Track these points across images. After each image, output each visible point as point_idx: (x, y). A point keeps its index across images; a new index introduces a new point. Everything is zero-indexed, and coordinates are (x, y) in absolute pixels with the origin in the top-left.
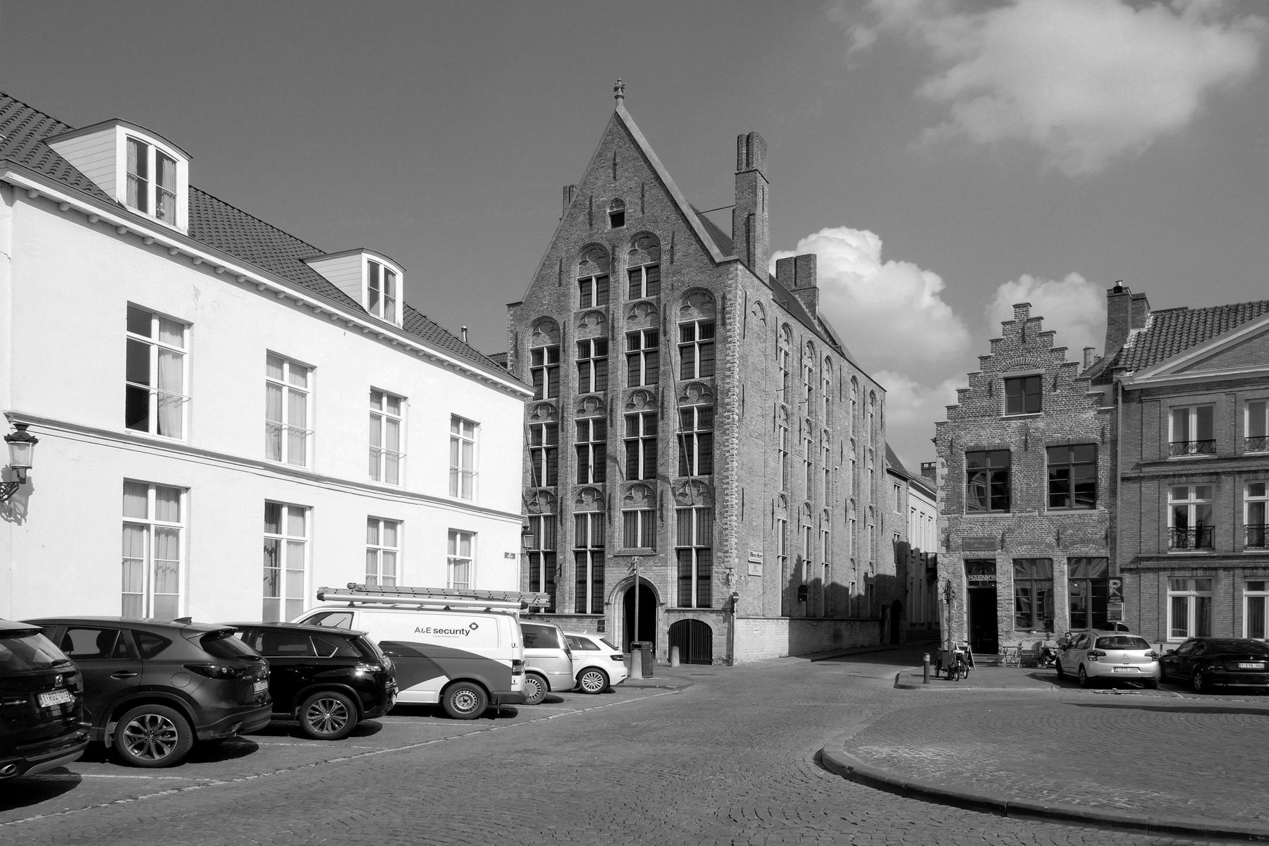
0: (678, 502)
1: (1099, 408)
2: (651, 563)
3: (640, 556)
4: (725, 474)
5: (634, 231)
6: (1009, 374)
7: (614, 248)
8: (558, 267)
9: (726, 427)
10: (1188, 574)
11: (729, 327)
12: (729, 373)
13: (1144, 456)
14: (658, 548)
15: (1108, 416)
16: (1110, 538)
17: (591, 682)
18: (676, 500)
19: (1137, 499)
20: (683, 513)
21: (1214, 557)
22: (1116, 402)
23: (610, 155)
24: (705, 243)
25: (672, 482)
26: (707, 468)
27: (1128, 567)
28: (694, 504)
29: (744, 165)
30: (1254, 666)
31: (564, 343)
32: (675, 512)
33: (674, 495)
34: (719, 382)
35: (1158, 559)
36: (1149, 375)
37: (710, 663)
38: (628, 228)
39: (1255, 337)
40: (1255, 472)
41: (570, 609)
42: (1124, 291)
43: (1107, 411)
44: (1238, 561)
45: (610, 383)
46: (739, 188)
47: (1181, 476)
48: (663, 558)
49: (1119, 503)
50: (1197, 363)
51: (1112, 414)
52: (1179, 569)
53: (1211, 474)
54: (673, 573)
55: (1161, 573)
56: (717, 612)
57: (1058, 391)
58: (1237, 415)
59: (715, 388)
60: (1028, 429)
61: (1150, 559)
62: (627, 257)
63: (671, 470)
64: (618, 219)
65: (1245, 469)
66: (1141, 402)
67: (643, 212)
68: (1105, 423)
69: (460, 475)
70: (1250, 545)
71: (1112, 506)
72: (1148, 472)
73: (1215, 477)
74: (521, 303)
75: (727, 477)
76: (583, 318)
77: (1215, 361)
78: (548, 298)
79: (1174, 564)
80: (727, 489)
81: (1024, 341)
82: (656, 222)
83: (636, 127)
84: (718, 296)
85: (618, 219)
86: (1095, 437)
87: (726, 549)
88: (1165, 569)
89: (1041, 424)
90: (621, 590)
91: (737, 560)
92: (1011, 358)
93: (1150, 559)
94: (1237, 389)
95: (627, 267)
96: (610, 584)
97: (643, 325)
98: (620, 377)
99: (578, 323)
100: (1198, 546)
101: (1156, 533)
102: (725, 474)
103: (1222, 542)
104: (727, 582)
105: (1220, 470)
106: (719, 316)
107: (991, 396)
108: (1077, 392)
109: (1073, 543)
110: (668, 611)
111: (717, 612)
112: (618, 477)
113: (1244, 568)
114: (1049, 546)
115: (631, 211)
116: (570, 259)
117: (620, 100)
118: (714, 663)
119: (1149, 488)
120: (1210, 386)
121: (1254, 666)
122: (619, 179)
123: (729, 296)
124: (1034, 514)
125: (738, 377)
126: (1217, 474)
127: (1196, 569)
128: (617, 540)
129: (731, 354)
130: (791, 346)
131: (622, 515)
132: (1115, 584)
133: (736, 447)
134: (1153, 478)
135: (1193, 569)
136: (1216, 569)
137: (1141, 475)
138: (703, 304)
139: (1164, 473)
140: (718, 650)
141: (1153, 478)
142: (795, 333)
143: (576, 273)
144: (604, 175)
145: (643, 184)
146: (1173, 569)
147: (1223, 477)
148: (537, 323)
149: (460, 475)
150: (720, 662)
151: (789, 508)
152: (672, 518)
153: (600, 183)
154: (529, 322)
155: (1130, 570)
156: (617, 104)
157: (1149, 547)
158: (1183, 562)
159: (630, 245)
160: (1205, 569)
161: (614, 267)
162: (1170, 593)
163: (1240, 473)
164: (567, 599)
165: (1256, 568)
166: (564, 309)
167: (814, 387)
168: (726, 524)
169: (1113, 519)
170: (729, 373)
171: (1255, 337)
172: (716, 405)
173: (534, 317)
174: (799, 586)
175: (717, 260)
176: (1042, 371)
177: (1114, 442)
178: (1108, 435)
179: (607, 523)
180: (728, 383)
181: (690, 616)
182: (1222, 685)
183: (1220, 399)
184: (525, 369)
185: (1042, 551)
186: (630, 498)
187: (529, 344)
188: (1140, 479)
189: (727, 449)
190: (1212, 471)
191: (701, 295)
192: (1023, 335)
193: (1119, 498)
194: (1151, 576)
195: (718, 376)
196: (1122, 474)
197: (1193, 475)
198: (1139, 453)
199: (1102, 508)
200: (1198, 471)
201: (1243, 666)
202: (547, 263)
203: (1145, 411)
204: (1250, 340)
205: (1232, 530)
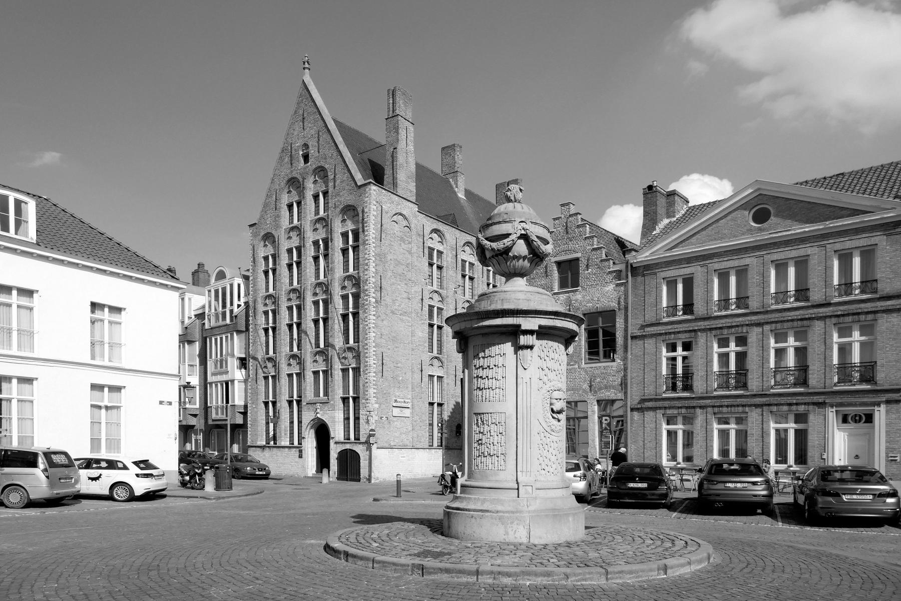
0: (342, 364)
1: (617, 282)
3: (321, 403)
4: (366, 342)
5: (314, 167)
6: (559, 259)
7: (304, 179)
8: (274, 197)
9: (366, 307)
10: (675, 412)
11: (366, 233)
12: (366, 267)
13: (646, 318)
14: (330, 397)
15: (622, 288)
16: (624, 385)
18: (341, 362)
19: (642, 353)
20: (345, 371)
21: (693, 398)
22: (627, 277)
23: (301, 112)
24: (353, 172)
25: (337, 349)
26: (357, 340)
27: (636, 407)
28: (350, 365)
29: (391, 112)
30: (640, 485)
31: (278, 251)
32: (340, 371)
33: (339, 358)
34: (361, 274)
35: (656, 400)
36: (647, 254)
37: (359, 480)
38: (312, 164)
39: (721, 219)
40: (721, 328)
42: (654, 189)
43: (622, 284)
44: (710, 401)
45: (303, 279)
46: (388, 131)
47: (670, 333)
48: (333, 404)
49: (630, 357)
50: (681, 242)
51: (625, 286)
52: (670, 408)
53: (690, 331)
54: (340, 415)
55: (658, 411)
56: (363, 443)
57: (590, 270)
58: (708, 283)
59: (359, 277)
60: (571, 301)
61: (650, 400)
63: (337, 340)
64: (306, 158)
65: (714, 326)
66: (644, 275)
67: (319, 152)
68: (621, 293)
69: (106, 346)
70: (720, 387)
71: (625, 359)
72: (648, 332)
73: (693, 334)
74: (255, 224)
75: (367, 344)
76: (289, 233)
77: (693, 240)
78: (269, 219)
79: (666, 404)
80: (367, 353)
81: (567, 233)
82: (325, 159)
83: (316, 90)
84: (360, 210)
85: (306, 158)
86: (614, 305)
87: (367, 397)
88: (660, 408)
89: (579, 296)
90: (311, 428)
91: (377, 406)
92: (559, 246)
93: (650, 400)
94: (708, 262)
95: (312, 193)
96: (305, 424)
97: (321, 235)
98: (308, 274)
99: (287, 237)
100: (736, 388)
101: (654, 380)
102: (366, 342)
103: (699, 386)
104: (368, 422)
105: (696, 328)
106: (361, 225)
107: (547, 276)
108: (602, 270)
109: (600, 389)
110: (336, 443)
111: (363, 443)
112: (308, 346)
113: (713, 407)
114: (584, 391)
115: (312, 152)
116: (282, 189)
117: (307, 70)
118: (362, 481)
119: (650, 344)
120: (689, 260)
121: (640, 485)
122: (306, 129)
123: (366, 210)
124: (575, 366)
125: (374, 270)
126: (695, 331)
127: (681, 408)
129: (368, 253)
130: (445, 246)
131: (312, 375)
132: (606, 420)
133: (373, 321)
134: (652, 336)
135: (679, 408)
136: (694, 407)
137: (644, 334)
138: (353, 217)
139: (659, 332)
140: (364, 472)
141: (652, 336)
142: (447, 236)
143: (285, 199)
144: (298, 126)
145: (319, 132)
146: (665, 408)
147: (699, 333)
148: (265, 238)
149: (106, 346)
150: (365, 480)
151: (445, 366)
152: (338, 375)
153: (296, 133)
154: (260, 237)
155: (637, 409)
156: (304, 74)
157: (650, 391)
158: (672, 403)
159: (313, 176)
160: (687, 408)
162: (773, 425)
163: (711, 329)
164: (283, 434)
165: (722, 406)
166: (278, 226)
168: (367, 379)
169: (625, 369)
170: (366, 267)
171: (721, 219)
173: (262, 234)
174: (456, 425)
175: (359, 184)
176: (579, 255)
177: (626, 308)
178: (623, 303)
179: (303, 380)
180: (366, 275)
181: (348, 446)
182: (616, 500)
183: (696, 270)
184: (259, 271)
185: (580, 395)
186: (315, 361)
187: (262, 253)
188: (642, 337)
189: (366, 323)
190: (691, 329)
191: (352, 211)
192: (566, 228)
193: (629, 353)
194: (651, 413)
195: (361, 270)
196: (632, 333)
197: (679, 332)
198: (643, 317)
199: (619, 361)
200: (681, 330)
201: (631, 485)
202: (269, 194)
203: (647, 283)
204: (717, 221)
205: (705, 376)
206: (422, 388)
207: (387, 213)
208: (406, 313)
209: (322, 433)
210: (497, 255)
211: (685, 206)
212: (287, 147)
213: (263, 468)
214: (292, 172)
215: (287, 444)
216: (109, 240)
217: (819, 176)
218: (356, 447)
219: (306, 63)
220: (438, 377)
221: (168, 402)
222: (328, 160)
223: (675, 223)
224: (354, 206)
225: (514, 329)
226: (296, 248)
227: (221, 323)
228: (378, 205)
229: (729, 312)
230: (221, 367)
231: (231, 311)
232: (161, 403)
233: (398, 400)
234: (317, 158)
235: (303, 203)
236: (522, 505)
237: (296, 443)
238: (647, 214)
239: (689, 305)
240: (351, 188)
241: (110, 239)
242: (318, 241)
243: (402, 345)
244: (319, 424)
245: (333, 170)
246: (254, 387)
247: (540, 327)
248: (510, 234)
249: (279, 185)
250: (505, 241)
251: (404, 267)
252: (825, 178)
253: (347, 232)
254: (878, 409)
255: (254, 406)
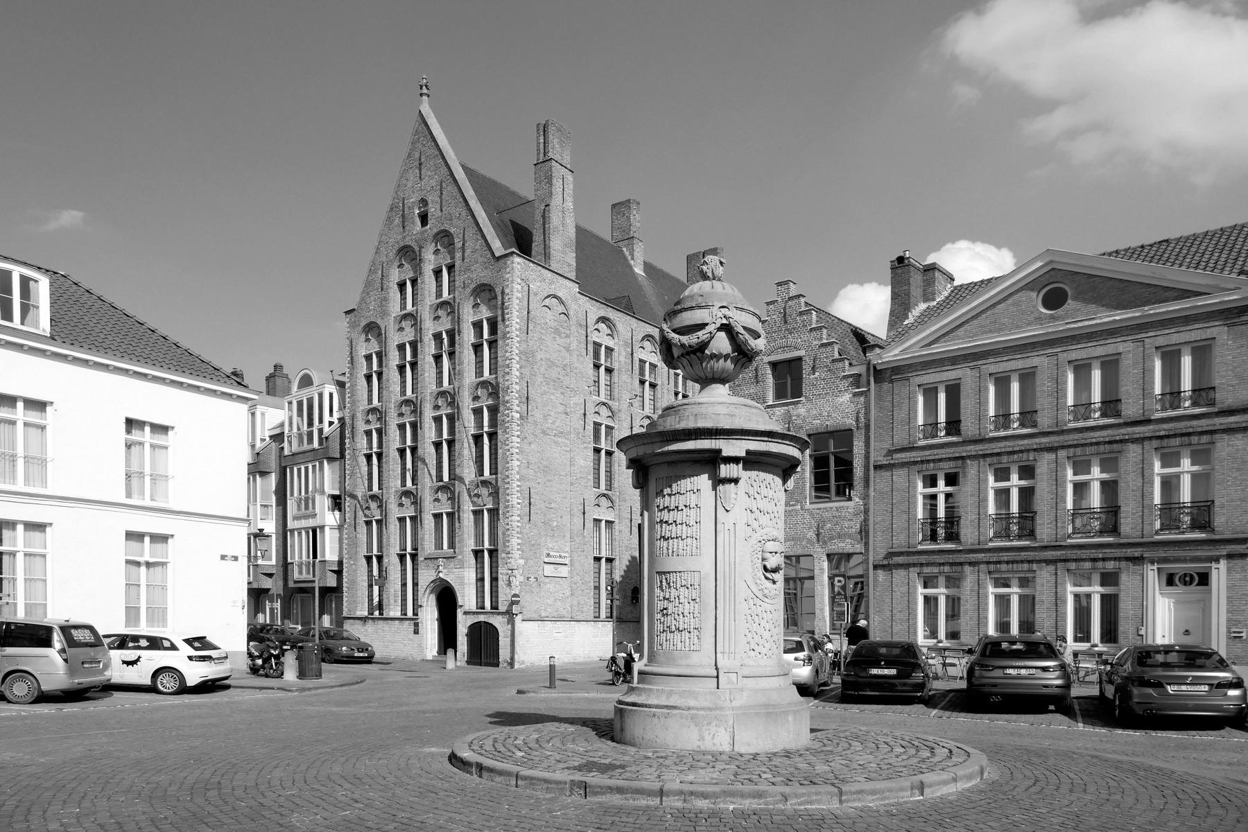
0: (474, 503)
1: (854, 391)
2: (452, 565)
3: (444, 558)
4: (507, 473)
5: (435, 231)
6: (774, 358)
7: (421, 248)
8: (380, 272)
9: (507, 425)
10: (935, 570)
11: (507, 323)
12: (507, 370)
13: (895, 441)
14: (457, 550)
15: (862, 399)
16: (864, 532)
17: (166, 683)
19: (889, 489)
20: (478, 514)
21: (960, 551)
22: (868, 383)
23: (417, 155)
24: (488, 238)
25: (467, 483)
26: (494, 470)
27: (881, 563)
28: (485, 505)
29: (542, 155)
30: (886, 672)
31: (385, 348)
32: (471, 513)
33: (470, 496)
34: (500, 380)
35: (909, 554)
36: (896, 351)
37: (497, 665)
38: (433, 227)
39: (999, 303)
40: (998, 454)
41: (397, 613)
42: (907, 262)
43: (861, 393)
44: (983, 555)
45: (419, 386)
46: (538, 181)
47: (928, 461)
48: (461, 560)
49: (872, 494)
50: (944, 335)
51: (866, 396)
52: (928, 564)
53: (956, 458)
54: (470, 575)
55: (911, 569)
56: (502, 613)
57: (817, 374)
58: (981, 391)
59: (498, 384)
60: (790, 417)
61: (901, 554)
62: (432, 257)
63: (466, 471)
64: (424, 219)
65: (989, 452)
66: (891, 381)
67: (442, 210)
68: (860, 406)
69: (147, 479)
70: (997, 536)
71: (865, 497)
72: (898, 459)
73: (960, 462)
74: (354, 310)
75: (508, 477)
76: (400, 322)
77: (960, 332)
78: (373, 303)
79: (923, 559)
80: (508, 488)
81: (786, 322)
82: (451, 220)
83: (438, 125)
84: (498, 290)
85: (424, 219)
86: (850, 422)
87: (508, 549)
88: (914, 565)
89: (801, 410)
90: (431, 592)
91: (522, 562)
92: (775, 341)
93: (901, 554)
94: (981, 362)
95: (432, 267)
96: (422, 587)
97: (445, 325)
98: (427, 379)
99: (397, 328)
101: (907, 526)
102: (507, 473)
103: (968, 534)
104: (509, 584)
105: (964, 454)
106: (500, 312)
107: (757, 382)
108: (834, 373)
109: (832, 538)
110: (466, 613)
111: (502, 613)
112: (427, 480)
113: (988, 563)
114: (809, 541)
115: (433, 210)
116: (390, 262)
117: (425, 98)
118: (501, 665)
119: (900, 476)
120: (954, 360)
121: (886, 672)
122: (424, 178)
123: (507, 291)
124: (796, 507)
126: (962, 458)
127: (943, 564)
128: (428, 546)
129: (510, 350)
130: (616, 340)
131: (432, 519)
132: (839, 581)
133: (517, 445)
134: (904, 465)
136: (961, 564)
137: (892, 462)
138: (489, 300)
139: (912, 460)
140: (504, 653)
141: (904, 465)
142: (620, 326)
143: (395, 275)
144: (413, 175)
145: (441, 183)
146: (922, 565)
147: (969, 462)
148: (367, 329)
149: (147, 479)
150: (505, 665)
151: (617, 507)
152: (468, 519)
153: (409, 184)
154: (360, 328)
155: (883, 567)
156: (421, 102)
157: (900, 542)
158: (931, 557)
159: (433, 244)
160: (951, 564)
161: (421, 268)
162: (1070, 589)
163: (984, 456)
164: (392, 601)
165: (999, 562)
166: (385, 313)
167: (659, 383)
168: (508, 524)
169: (866, 511)
170: (507, 370)
171: (999, 303)
172: (499, 403)
173: (363, 323)
174: (632, 588)
175: (497, 254)
176: (802, 353)
177: (867, 427)
178: (862, 420)
179: (419, 526)
180: (507, 380)
181: (482, 618)
182: (853, 693)
183: (964, 374)
184: (359, 375)
185: (803, 548)
186: (437, 500)
187: (362, 350)
188: (890, 467)
189: (507, 447)
190: (957, 455)
191: (487, 293)
192: (785, 316)
193: (872, 489)
194: (902, 572)
195: (500, 373)
196: (875, 461)
197: (940, 460)
198: (890, 439)
199: (857, 500)
200: (944, 456)
201: (875, 671)
202: (373, 268)
203: (896, 391)
204: (994, 305)
205: (977, 521)
206: (584, 537)
207: (536, 294)
208: (562, 433)
209: (446, 599)
210: (688, 353)
211: (949, 286)
212: (398, 203)
213: (364, 648)
214: (404, 238)
215: (398, 614)
216: (151, 332)
217: (1135, 243)
218: (493, 619)
219: (424, 87)
220: (606, 521)
221: (233, 557)
222: (454, 222)
223: (935, 309)
224: (490, 285)
225: (712, 455)
226: (410, 343)
227: (306, 447)
228: (523, 284)
229: (1010, 432)
230: (307, 508)
231: (321, 431)
232: (223, 557)
233: (551, 553)
234: (439, 219)
235: (419, 281)
236: (723, 699)
237: (410, 613)
238: (896, 296)
239: (955, 422)
240: (485, 260)
241: (153, 331)
242: (441, 333)
243: (556, 478)
244: (442, 587)
245: (461, 236)
246: (351, 535)
247: (748, 452)
248: (707, 324)
249: (387, 256)
250: (700, 333)
251: (559, 369)
252: (1142, 247)
253: (481, 321)
254: (1217, 566)
255: (352, 562)
